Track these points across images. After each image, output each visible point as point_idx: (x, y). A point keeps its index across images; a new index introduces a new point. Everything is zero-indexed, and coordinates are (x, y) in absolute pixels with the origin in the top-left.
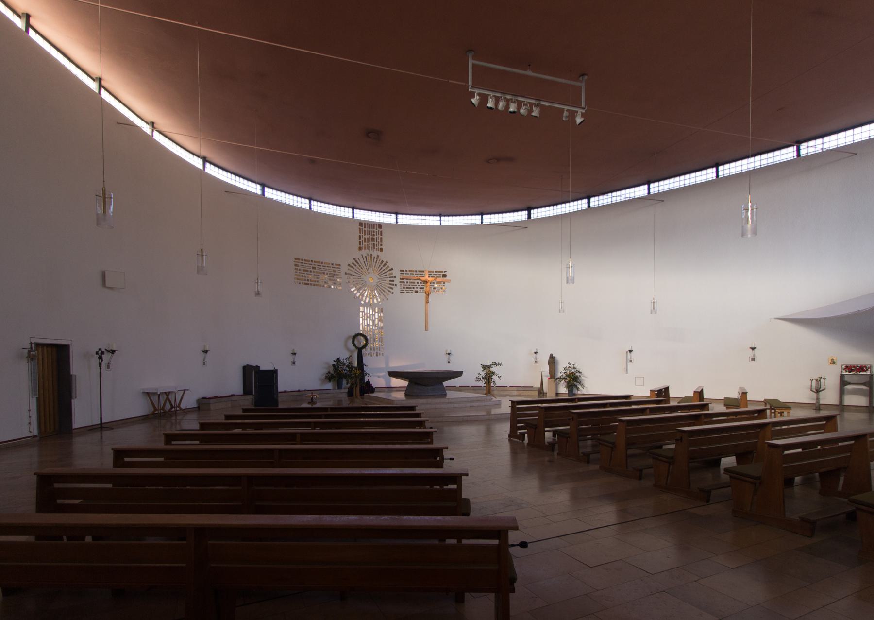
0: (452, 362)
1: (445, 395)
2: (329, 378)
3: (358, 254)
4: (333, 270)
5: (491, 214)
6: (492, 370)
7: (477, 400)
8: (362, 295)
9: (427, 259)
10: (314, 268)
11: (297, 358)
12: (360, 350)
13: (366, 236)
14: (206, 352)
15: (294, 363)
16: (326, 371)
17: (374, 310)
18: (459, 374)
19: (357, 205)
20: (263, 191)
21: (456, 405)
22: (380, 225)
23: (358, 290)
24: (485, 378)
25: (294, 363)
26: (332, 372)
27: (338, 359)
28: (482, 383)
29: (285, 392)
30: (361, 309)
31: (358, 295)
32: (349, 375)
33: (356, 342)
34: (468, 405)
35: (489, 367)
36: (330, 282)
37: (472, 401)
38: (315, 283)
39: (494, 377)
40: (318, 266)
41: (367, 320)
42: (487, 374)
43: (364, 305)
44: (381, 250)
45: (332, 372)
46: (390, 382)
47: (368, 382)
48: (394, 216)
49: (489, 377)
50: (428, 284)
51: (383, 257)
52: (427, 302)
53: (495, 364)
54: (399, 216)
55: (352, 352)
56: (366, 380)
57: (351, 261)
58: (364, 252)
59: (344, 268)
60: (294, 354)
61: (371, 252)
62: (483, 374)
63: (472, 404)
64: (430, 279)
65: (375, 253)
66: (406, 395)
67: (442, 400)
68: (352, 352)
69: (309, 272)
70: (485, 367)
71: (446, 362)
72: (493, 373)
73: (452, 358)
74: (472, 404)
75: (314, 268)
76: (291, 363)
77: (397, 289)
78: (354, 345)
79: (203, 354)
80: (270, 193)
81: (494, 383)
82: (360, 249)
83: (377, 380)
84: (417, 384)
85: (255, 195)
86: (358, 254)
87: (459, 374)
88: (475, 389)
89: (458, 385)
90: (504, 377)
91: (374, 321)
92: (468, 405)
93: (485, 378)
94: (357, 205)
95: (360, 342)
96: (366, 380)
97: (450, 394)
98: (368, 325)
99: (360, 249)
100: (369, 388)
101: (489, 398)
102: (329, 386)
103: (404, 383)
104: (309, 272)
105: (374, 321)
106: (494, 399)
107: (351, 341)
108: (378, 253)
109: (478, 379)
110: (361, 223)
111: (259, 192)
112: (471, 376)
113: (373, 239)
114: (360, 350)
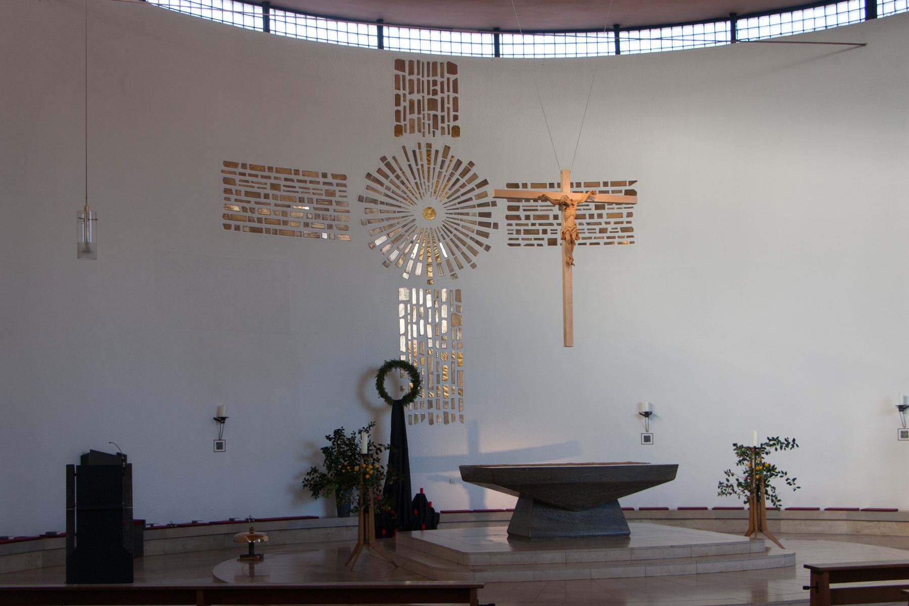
0: (655, 439)
1: (626, 536)
2: (315, 485)
3: (392, 147)
4: (327, 191)
5: (758, 14)
6: (767, 459)
7: (722, 553)
8: (405, 256)
9: (573, 151)
10: (275, 187)
11: (229, 432)
12: (398, 408)
13: (416, 97)
14: (221, 420)
15: (219, 446)
16: (306, 466)
17: (437, 298)
18: (666, 473)
19: (388, 13)
20: (266, 20)
21: (653, 570)
22: (452, 66)
23: (395, 241)
24: (745, 486)
25: (219, 446)
26: (323, 470)
27: (338, 433)
28: (738, 500)
29: (195, 524)
30: (403, 294)
31: (393, 256)
32: (368, 484)
33: (387, 385)
34: (691, 568)
35: (757, 452)
36: (318, 225)
37: (705, 557)
38: (278, 228)
39: (773, 481)
40: (288, 182)
41: (415, 325)
42: (751, 472)
43: (409, 285)
44: (456, 131)
45: (323, 470)
46: (482, 497)
47: (421, 497)
48: (489, 38)
49: (758, 480)
50: (571, 211)
51: (460, 149)
52: (569, 263)
53: (774, 442)
54: (505, 38)
55: (377, 412)
56: (415, 491)
57: (373, 166)
58: (410, 140)
59: (357, 185)
60: (221, 420)
61: (429, 138)
62: (740, 472)
63: (704, 567)
64: (577, 197)
65: (439, 141)
66: (512, 536)
67: (614, 554)
68: (377, 412)
69: (260, 197)
70: (745, 453)
71: (639, 439)
72: (771, 470)
73: (655, 428)
74: (704, 567)
75: (275, 187)
76: (212, 446)
77: (498, 238)
78: (383, 394)
79: (216, 426)
80: (285, 25)
81: (775, 499)
82: (399, 131)
83: (447, 493)
84: (538, 503)
85: (253, 33)
86: (392, 147)
87: (666, 473)
88: (720, 517)
89: (673, 505)
90: (804, 482)
91: (436, 327)
92: (691, 568)
93: (745, 486)
94: (388, 13)
95: (398, 386)
96: (415, 491)
97: (643, 535)
98: (422, 339)
99: (399, 131)
100: (423, 514)
101: (756, 547)
102: (316, 507)
103: (502, 500)
104: (260, 197)
105: (436, 327)
106: (775, 551)
107: (374, 381)
108: (448, 139)
109: (725, 489)
110: (401, 62)
111: (259, 24)
112: (704, 477)
113: (432, 104)
114: (398, 408)
